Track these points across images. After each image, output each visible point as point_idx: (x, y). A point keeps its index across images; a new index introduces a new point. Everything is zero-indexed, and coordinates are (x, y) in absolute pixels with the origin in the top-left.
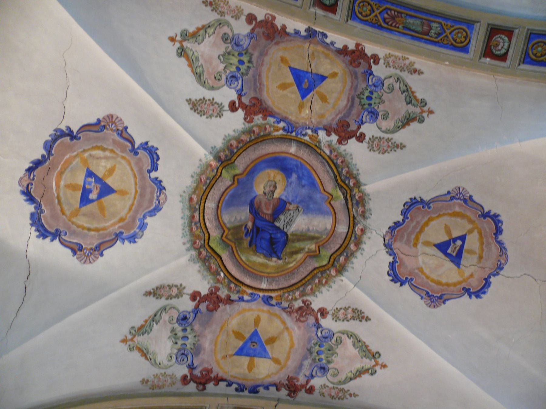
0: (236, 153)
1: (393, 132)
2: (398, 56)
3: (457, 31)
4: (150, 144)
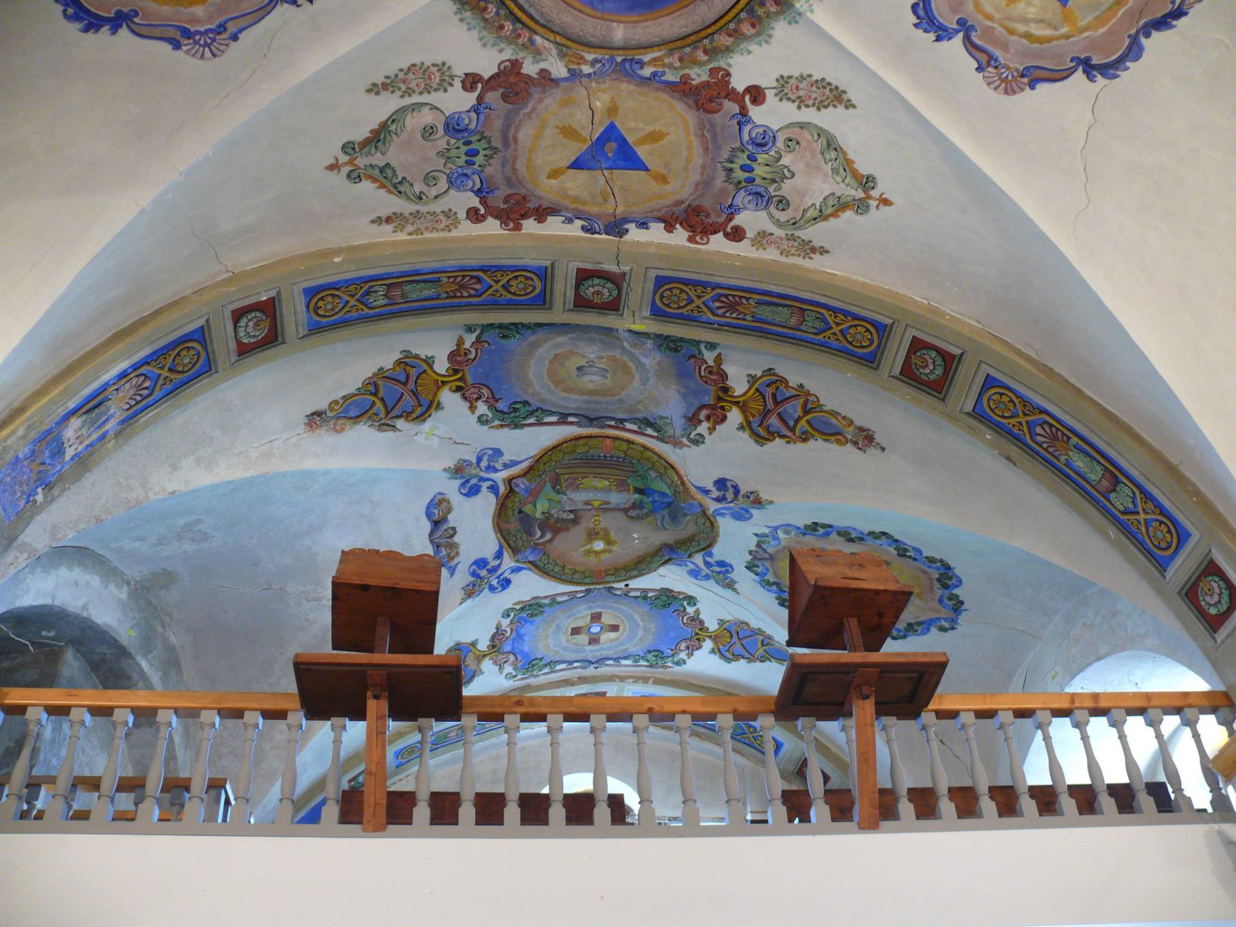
0: (742, 10)
1: (403, 110)
2: (432, 231)
3: (337, 310)
4: (932, 36)
